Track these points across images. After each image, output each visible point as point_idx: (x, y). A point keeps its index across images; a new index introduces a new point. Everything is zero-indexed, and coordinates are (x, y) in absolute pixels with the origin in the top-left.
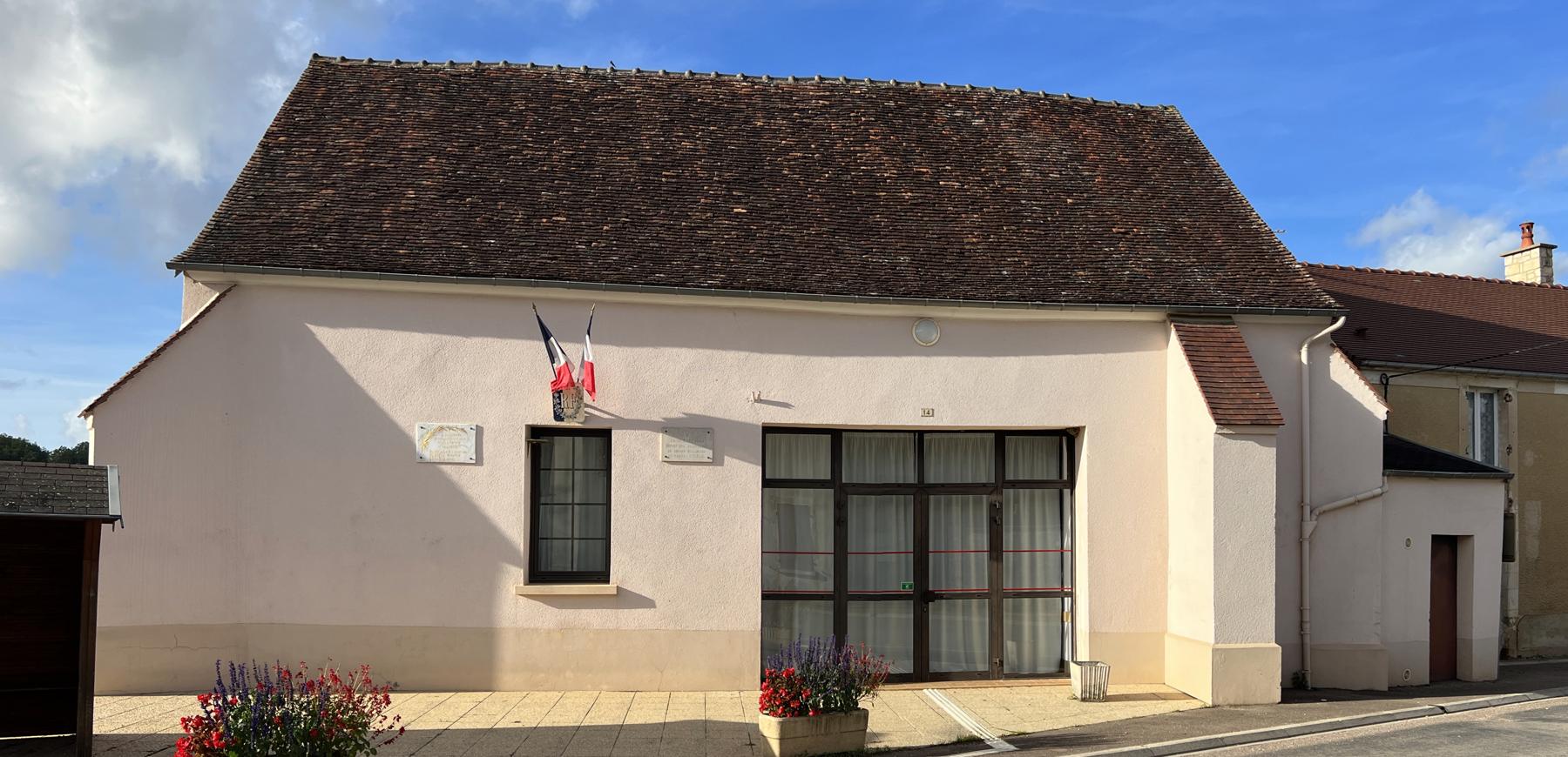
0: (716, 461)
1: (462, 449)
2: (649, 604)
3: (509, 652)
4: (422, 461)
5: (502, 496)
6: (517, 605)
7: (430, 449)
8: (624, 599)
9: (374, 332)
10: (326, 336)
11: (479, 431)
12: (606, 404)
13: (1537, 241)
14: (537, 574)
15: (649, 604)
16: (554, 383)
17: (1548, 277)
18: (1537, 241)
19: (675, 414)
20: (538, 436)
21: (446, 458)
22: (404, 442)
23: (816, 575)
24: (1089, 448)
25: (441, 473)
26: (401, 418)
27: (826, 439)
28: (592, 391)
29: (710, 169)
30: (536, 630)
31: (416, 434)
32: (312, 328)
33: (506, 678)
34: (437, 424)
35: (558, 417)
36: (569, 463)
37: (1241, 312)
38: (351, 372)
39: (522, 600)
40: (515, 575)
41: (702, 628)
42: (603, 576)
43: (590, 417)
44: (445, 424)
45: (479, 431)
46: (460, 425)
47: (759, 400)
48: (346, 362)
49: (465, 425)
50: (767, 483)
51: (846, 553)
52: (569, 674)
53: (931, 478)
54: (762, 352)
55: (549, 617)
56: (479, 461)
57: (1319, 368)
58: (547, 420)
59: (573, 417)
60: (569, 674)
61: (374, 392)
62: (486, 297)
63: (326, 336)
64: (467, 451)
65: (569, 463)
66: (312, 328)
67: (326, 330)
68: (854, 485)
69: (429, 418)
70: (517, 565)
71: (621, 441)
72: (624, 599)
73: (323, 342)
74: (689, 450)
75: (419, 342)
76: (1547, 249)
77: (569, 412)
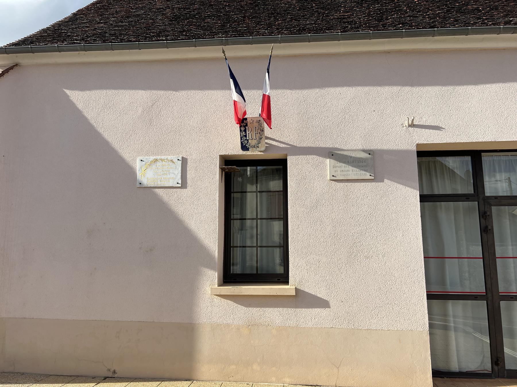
1: (172, 175)
2: (324, 304)
3: (206, 345)
4: (142, 187)
5: (202, 214)
6: (213, 304)
7: (146, 176)
8: (302, 299)
9: (110, 92)
10: (77, 97)
11: (184, 161)
12: (282, 133)
14: (229, 277)
15: (324, 304)
20: (231, 167)
21: (160, 184)
22: (131, 172)
25: (156, 196)
26: (126, 155)
28: (269, 125)
29: (385, 240)
30: (228, 325)
31: (138, 165)
32: (68, 92)
33: (205, 369)
34: (152, 158)
35: (244, 148)
36: (253, 182)
38: (92, 122)
39: (217, 299)
40: (211, 278)
41: (374, 327)
42: (283, 278)
43: (269, 147)
44: (158, 157)
45: (184, 161)
46: (170, 158)
47: (412, 125)
48: (90, 115)
49: (174, 158)
50: (423, 198)
52: (255, 367)
54: (412, 85)
55: (241, 313)
56: (184, 185)
58: (234, 149)
59: (256, 147)
60: (255, 367)
61: (108, 135)
62: (186, 60)
63: (77, 97)
64: (175, 179)
65: (253, 182)
66: (68, 92)
67: (77, 93)
68: (496, 198)
69: (147, 154)
70: (213, 268)
71: (291, 161)
72: (302, 299)
73: (75, 101)
74: (353, 172)
75: (141, 97)
77: (252, 142)
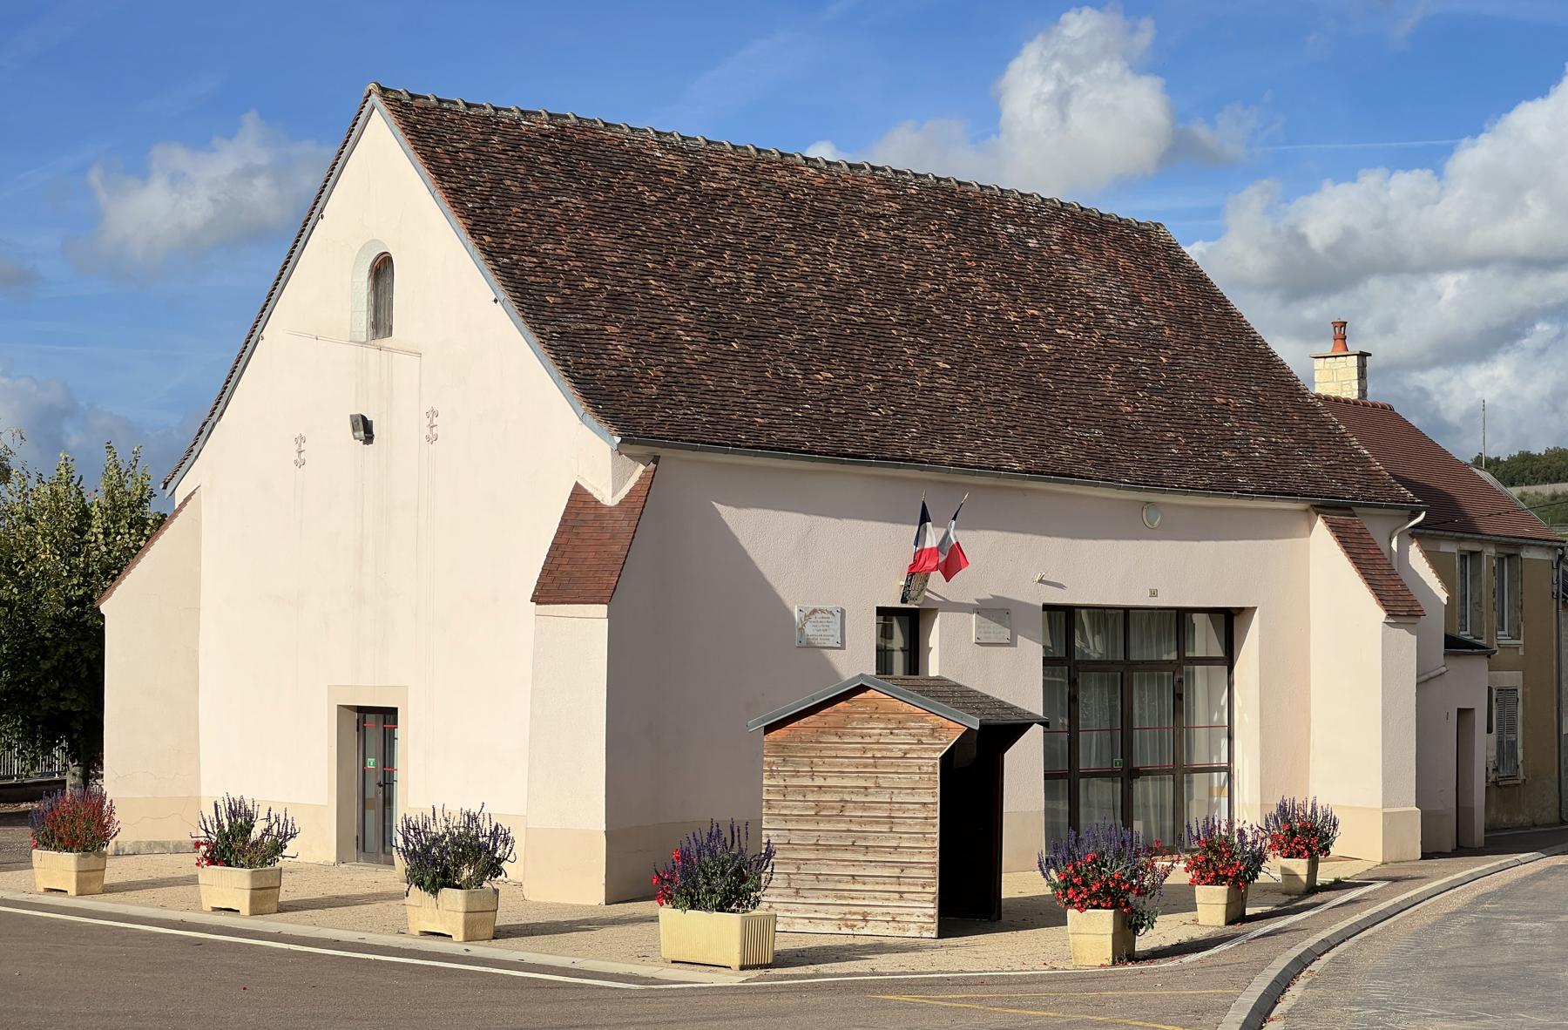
0: (1012, 643)
10: (727, 513)
11: (843, 612)
13: (1354, 347)
16: (912, 567)
17: (1363, 391)
18: (1354, 347)
19: (986, 596)
23: (1063, 766)
24: (1261, 619)
25: (827, 662)
27: (1222, 616)
32: (718, 506)
37: (1360, 505)
47: (1041, 581)
51: (1132, 729)
53: (1135, 656)
56: (843, 647)
57: (1403, 552)
63: (727, 513)
66: (718, 506)
76: (1363, 356)
